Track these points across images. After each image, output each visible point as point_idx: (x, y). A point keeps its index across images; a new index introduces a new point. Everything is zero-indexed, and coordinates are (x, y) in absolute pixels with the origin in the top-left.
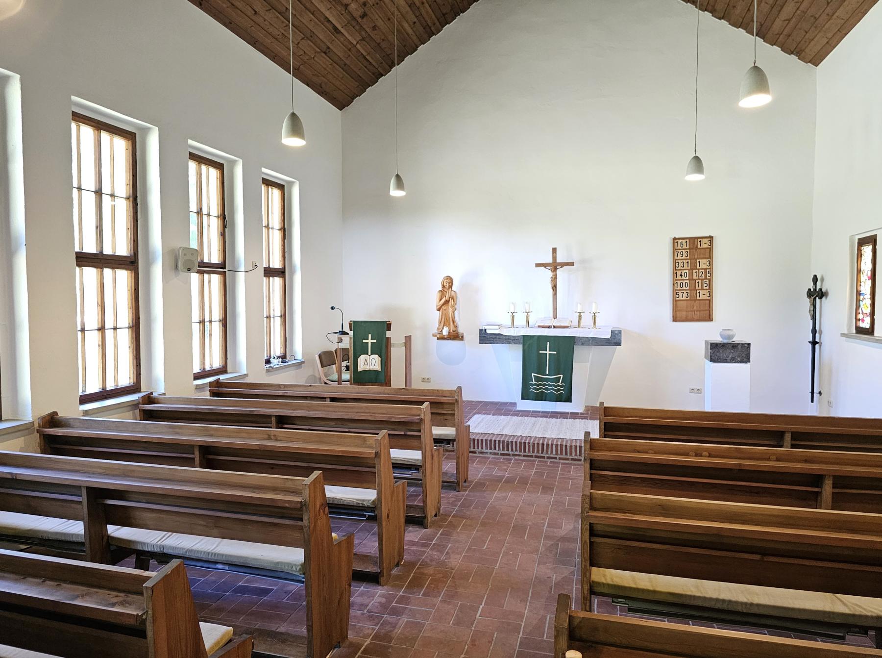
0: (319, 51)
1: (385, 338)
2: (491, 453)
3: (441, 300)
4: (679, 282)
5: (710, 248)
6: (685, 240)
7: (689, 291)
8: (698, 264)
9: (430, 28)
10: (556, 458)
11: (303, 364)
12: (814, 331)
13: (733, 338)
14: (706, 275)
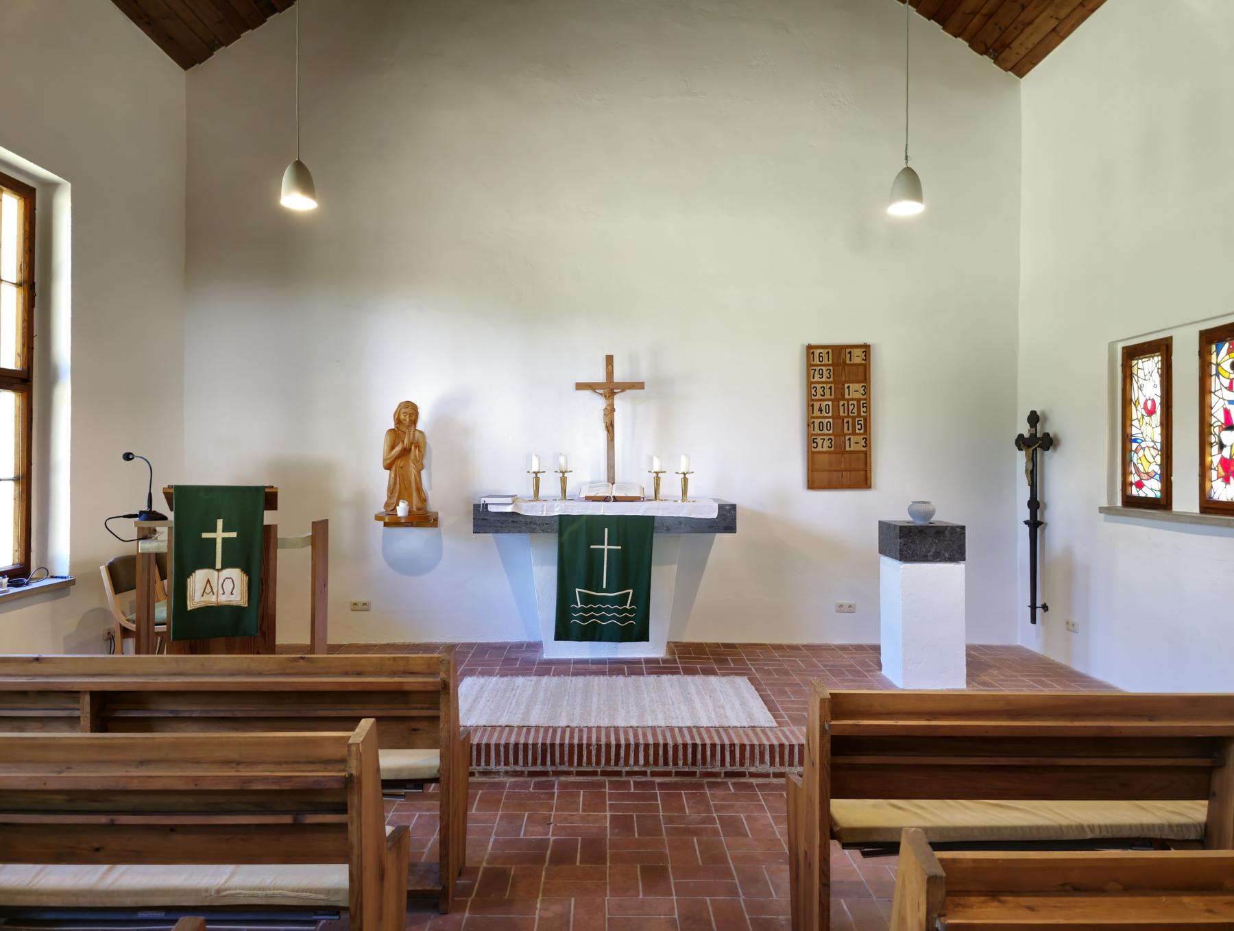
2: (506, 773)
3: (393, 448)
4: (817, 421)
5: (865, 365)
6: (827, 351)
7: (832, 437)
8: (846, 390)
10: (644, 773)
11: (72, 587)
13: (931, 517)
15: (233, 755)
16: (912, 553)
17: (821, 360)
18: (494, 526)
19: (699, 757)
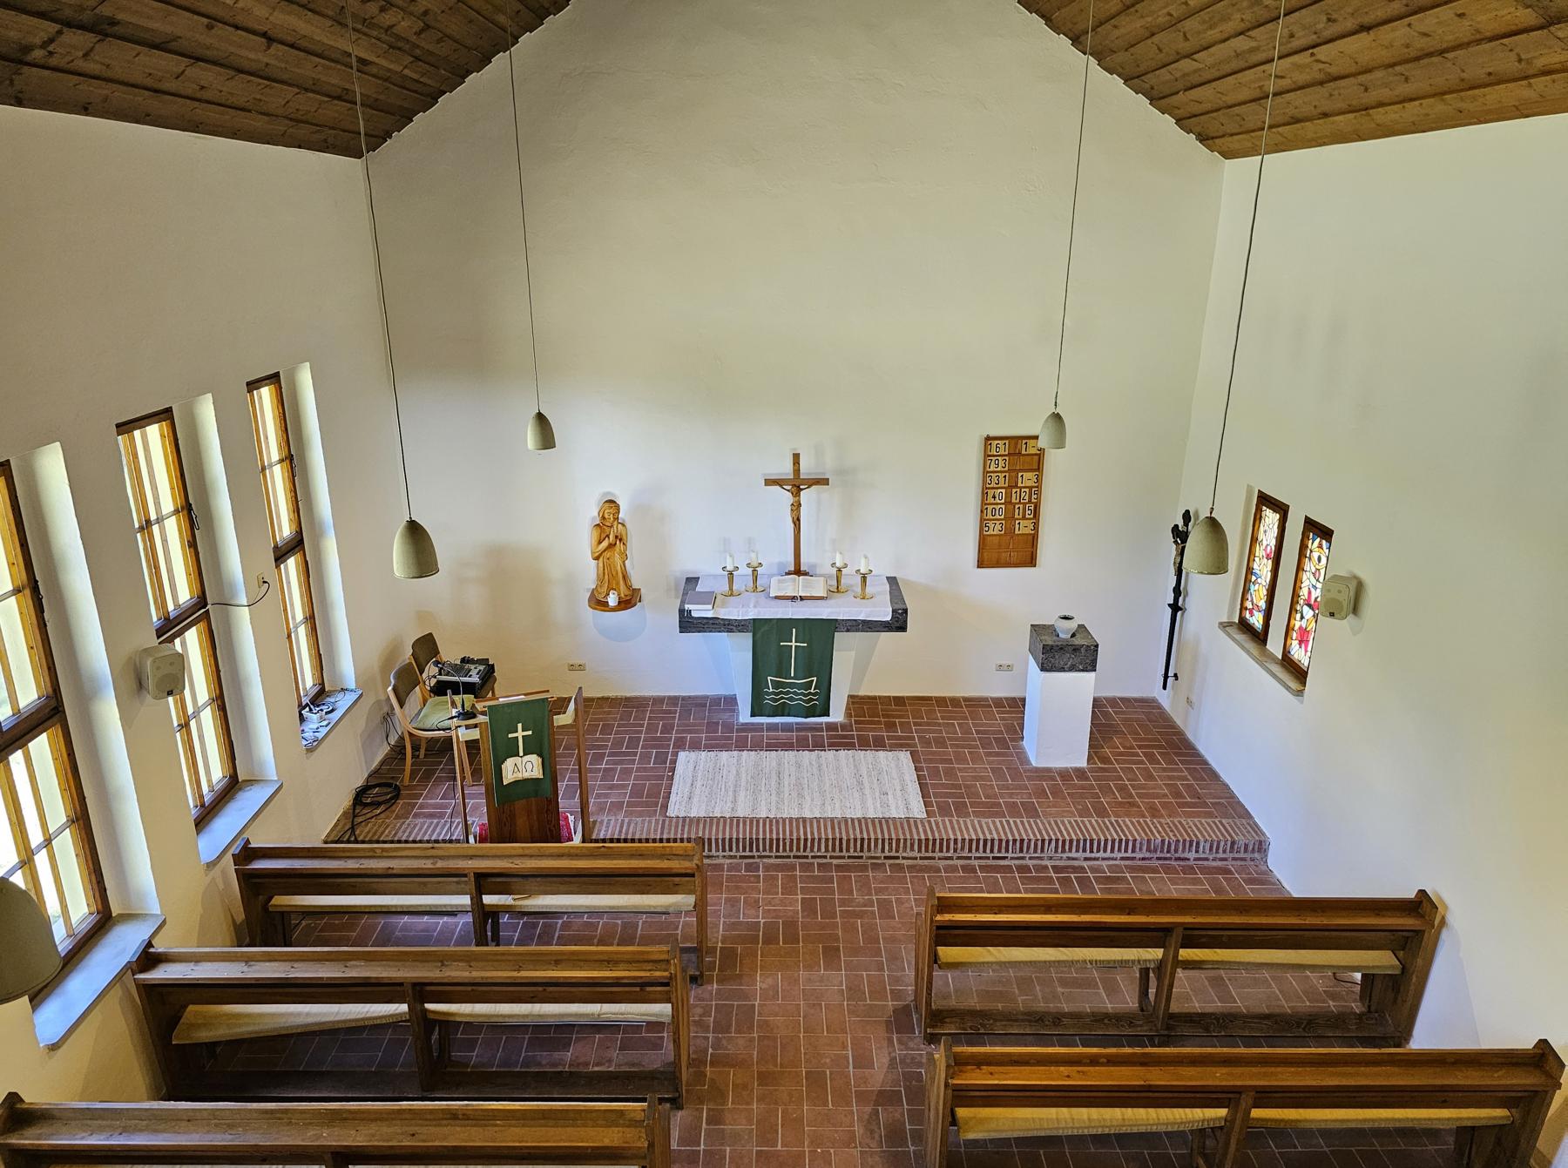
2: (724, 856)
4: (990, 507)
8: (1020, 479)
10: (825, 857)
12: (1177, 591)
19: (866, 846)
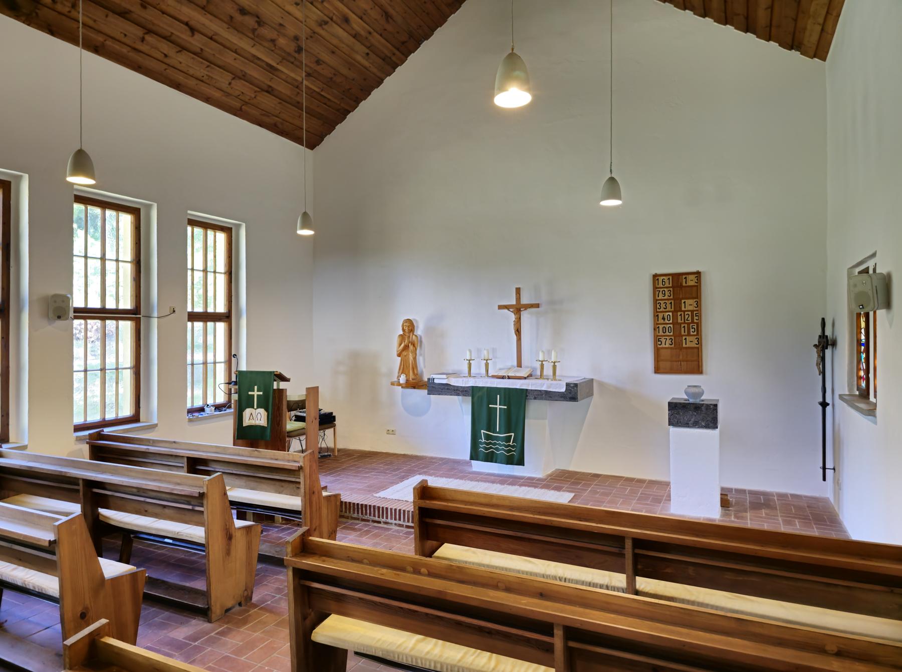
0: (259, 90)
1: (272, 389)
2: (395, 524)
5: (697, 286)
7: (673, 338)
8: (683, 305)
9: (390, 58)
14: (693, 319)
15: (179, 481)
16: (677, 421)
17: (664, 284)
18: (438, 391)
